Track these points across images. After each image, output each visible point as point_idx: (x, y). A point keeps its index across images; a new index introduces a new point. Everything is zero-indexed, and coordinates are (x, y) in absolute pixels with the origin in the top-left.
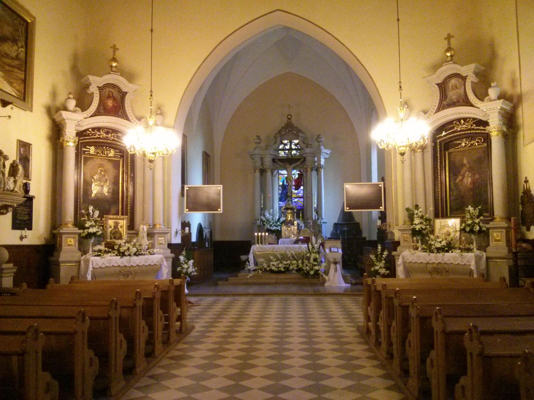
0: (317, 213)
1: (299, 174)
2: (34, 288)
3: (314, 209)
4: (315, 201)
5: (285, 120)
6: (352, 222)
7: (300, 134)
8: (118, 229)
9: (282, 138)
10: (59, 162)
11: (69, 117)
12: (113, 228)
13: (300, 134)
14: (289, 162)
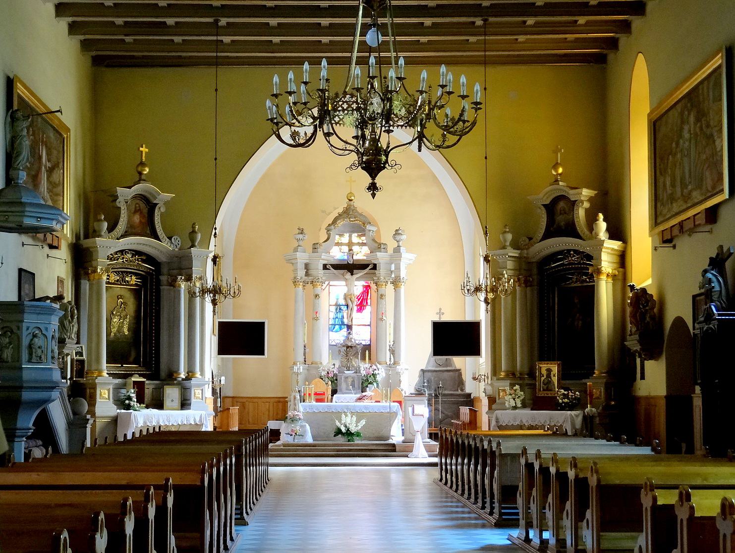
0: (393, 352)
3: (388, 348)
4: (390, 330)
6: (449, 368)
7: (368, 227)
8: (551, 378)
10: (497, 340)
11: (628, 344)
12: (545, 377)
13: (368, 227)
14: (350, 267)
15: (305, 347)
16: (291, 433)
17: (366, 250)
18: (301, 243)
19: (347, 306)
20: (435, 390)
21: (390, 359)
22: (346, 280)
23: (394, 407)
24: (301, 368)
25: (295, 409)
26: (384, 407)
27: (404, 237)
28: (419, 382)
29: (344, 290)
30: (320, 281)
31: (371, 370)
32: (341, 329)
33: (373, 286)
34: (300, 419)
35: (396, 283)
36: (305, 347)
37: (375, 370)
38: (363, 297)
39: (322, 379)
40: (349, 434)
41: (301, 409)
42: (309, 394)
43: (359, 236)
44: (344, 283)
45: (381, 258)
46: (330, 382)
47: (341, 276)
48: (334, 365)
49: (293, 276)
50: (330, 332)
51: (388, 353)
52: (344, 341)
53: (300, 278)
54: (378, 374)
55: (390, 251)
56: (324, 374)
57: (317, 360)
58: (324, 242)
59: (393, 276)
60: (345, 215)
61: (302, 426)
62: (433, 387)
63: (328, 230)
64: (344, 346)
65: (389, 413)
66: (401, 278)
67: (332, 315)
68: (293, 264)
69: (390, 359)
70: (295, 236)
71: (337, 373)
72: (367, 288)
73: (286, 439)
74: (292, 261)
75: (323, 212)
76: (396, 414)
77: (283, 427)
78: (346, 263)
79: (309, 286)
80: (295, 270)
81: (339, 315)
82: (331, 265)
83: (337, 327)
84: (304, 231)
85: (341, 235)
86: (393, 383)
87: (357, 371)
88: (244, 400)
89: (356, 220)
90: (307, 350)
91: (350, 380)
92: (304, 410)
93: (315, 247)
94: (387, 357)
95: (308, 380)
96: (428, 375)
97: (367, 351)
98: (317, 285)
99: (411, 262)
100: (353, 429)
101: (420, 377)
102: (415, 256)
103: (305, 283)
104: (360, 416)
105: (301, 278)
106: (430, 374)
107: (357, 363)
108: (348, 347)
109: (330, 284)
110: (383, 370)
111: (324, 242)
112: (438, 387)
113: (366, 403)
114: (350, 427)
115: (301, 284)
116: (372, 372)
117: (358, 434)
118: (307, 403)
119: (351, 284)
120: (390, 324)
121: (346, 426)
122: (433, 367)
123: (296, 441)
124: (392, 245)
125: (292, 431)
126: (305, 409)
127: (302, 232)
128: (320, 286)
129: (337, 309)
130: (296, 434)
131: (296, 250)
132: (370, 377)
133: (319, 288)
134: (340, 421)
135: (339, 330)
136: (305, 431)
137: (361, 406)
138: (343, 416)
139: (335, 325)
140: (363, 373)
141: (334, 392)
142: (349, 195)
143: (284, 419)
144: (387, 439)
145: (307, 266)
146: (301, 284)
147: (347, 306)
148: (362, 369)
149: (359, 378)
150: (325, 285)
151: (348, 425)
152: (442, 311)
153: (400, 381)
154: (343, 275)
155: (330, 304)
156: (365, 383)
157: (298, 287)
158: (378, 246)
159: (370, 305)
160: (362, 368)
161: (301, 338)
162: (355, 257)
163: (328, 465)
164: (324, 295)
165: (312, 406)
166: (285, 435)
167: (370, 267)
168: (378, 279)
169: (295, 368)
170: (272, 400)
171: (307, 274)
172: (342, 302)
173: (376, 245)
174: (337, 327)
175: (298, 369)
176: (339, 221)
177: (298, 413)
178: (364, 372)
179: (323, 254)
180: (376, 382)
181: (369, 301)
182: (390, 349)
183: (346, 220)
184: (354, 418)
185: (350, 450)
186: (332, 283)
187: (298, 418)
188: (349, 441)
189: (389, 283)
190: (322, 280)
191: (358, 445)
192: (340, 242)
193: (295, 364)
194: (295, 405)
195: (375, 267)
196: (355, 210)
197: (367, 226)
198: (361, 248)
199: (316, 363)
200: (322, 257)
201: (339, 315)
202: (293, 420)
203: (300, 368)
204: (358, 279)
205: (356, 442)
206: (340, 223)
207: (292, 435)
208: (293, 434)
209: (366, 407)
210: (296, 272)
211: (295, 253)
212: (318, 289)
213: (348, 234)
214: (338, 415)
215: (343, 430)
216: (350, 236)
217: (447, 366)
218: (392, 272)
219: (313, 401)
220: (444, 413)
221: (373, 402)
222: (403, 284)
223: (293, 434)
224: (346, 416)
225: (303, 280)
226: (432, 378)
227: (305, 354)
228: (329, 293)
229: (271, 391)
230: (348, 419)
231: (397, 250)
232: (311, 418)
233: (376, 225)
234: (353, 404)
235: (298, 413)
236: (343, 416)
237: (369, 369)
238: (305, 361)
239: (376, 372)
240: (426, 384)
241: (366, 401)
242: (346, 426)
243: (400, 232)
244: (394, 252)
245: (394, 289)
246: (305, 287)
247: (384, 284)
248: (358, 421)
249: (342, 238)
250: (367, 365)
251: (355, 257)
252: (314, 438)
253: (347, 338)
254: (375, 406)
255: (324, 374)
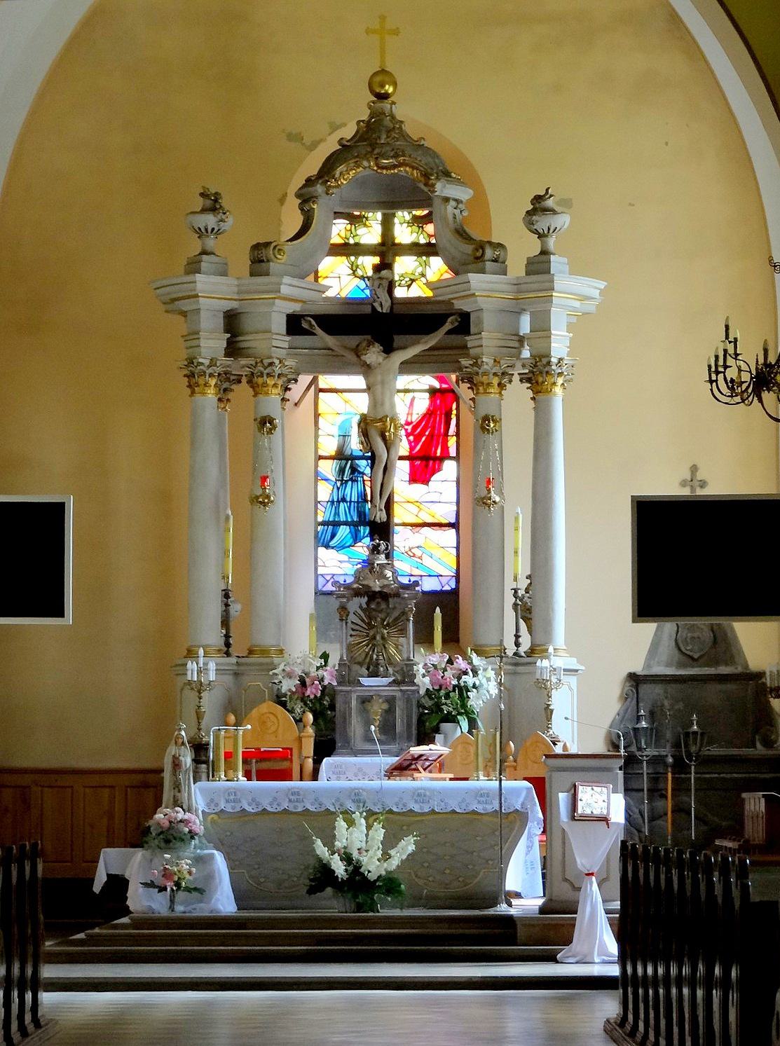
0: (525, 612)
1: (433, 392)
2: (394, 77)
3: (509, 600)
4: (518, 540)
5: (359, 109)
6: (724, 670)
7: (442, 188)
9: (331, 701)
13: (442, 188)
14: (374, 328)
15: (227, 596)
16: (160, 881)
17: (437, 268)
18: (211, 243)
19: (373, 459)
20: (677, 745)
21: (517, 637)
22: (366, 370)
23: (516, 791)
24: (212, 666)
25: (176, 803)
26: (481, 794)
27: (562, 221)
28: (622, 716)
29: (361, 403)
30: (277, 370)
31: (449, 674)
32: (356, 539)
33: (464, 391)
34: (192, 835)
35: (538, 375)
36: (227, 596)
37: (465, 673)
38: (433, 428)
39: (283, 704)
40: (358, 885)
41: (199, 802)
42: (228, 755)
43: (419, 222)
44: (358, 381)
45: (484, 289)
46: (310, 717)
47: (351, 357)
48: (325, 656)
49: (184, 354)
50: (322, 550)
51: (510, 615)
52: (358, 576)
53: (207, 362)
54: (474, 686)
55: (516, 268)
56: (288, 685)
57: (266, 639)
58: (291, 240)
59: (526, 353)
60: (363, 148)
61: (199, 860)
62: (669, 735)
63: (306, 199)
64: (357, 593)
65: (498, 813)
66: (554, 360)
67: (325, 492)
68: (184, 314)
69: (517, 637)
70: (191, 217)
71: (335, 683)
72: (442, 399)
73: (146, 903)
74: (179, 305)
75: (295, 137)
76: (518, 819)
77: (133, 865)
78: (368, 310)
79: (243, 389)
80: (193, 335)
81: (352, 492)
82: (315, 317)
83: (343, 531)
84: (224, 202)
85: (355, 220)
86: (524, 714)
87: (406, 676)
88: (26, 780)
89: (401, 165)
90: (235, 609)
91: (378, 708)
92: (208, 805)
93: (260, 257)
94: (509, 630)
95: (235, 708)
96: (651, 692)
97: (438, 610)
98: (265, 385)
99: (590, 306)
100: (373, 867)
101: (625, 698)
102: (602, 285)
103: (227, 381)
104: (397, 823)
105: (213, 362)
106: (658, 690)
107: (404, 649)
108: (372, 596)
109: (322, 385)
110: (491, 674)
111: (291, 240)
112: (687, 735)
113: (423, 780)
114: (364, 860)
115: (213, 382)
116: (455, 682)
117: (389, 884)
118: (221, 784)
119: (383, 383)
120: (517, 519)
121: (347, 858)
122: (668, 665)
123: (179, 908)
124: (520, 247)
125: (167, 874)
126: (210, 802)
127: (213, 204)
128: (275, 391)
129: (341, 471)
130: (178, 884)
131: (193, 267)
132: (447, 696)
133: (275, 394)
134: (329, 841)
135: (350, 542)
136: (210, 877)
137: (404, 791)
138: (341, 824)
139: (336, 524)
140: (424, 682)
141: (324, 748)
142: (378, 79)
143: (137, 837)
144: (494, 902)
145: (232, 322)
146: (213, 382)
147: (373, 459)
148: (420, 669)
149: (408, 701)
150: (297, 390)
151: (355, 855)
152: (699, 476)
153: (548, 712)
154: (357, 352)
155: (321, 453)
156: (432, 716)
157: (204, 394)
158: (473, 252)
159: (457, 458)
160: (421, 666)
161: (212, 569)
162: (400, 293)
163: (339, 983)
164: (294, 422)
165: (235, 792)
166: (141, 889)
167: (448, 326)
168: (475, 364)
169: (192, 666)
170: (126, 780)
171: (233, 350)
172: (355, 445)
173: (469, 249)
174: (343, 531)
175: (199, 672)
176: (342, 168)
177: (187, 816)
178: (427, 680)
179: (287, 280)
180: (469, 714)
181: (452, 442)
182: (515, 605)
183: (365, 163)
184: (379, 833)
185: (273, 940)
186: (325, 381)
187: (187, 830)
188: (359, 908)
189: (516, 378)
190: (285, 370)
191: (390, 922)
192: (352, 241)
193: (191, 654)
194: (177, 786)
195: (464, 324)
196: (396, 128)
197: (438, 186)
198: (426, 264)
199: (265, 652)
200: (285, 290)
201: (352, 492)
202: (172, 838)
203: (207, 668)
204: (408, 367)
205: (384, 912)
206: (347, 175)
207: (165, 889)
208: (170, 885)
209: (419, 795)
210: (194, 343)
211: (189, 278)
212: (271, 403)
213: (379, 215)
214: (323, 822)
215: (339, 868)
216: (387, 224)
217: (716, 663)
218: (521, 340)
219: (240, 774)
220: (705, 823)
221: (446, 780)
222: (560, 381)
223: (170, 885)
224: (351, 823)
225: (219, 370)
226: (666, 703)
227: (225, 622)
228: (317, 416)
229: (104, 746)
230: (355, 835)
231: (539, 265)
232: (236, 833)
233: (470, 179)
234: (376, 784)
235: (187, 816)
236: (341, 824)
237: (445, 670)
238: (228, 645)
239: (469, 680)
240: (644, 724)
241: (424, 774)
242: (347, 858)
243: (550, 203)
244: (528, 273)
245: (533, 399)
246: (230, 396)
247: (495, 381)
248: (390, 842)
249: (361, 231)
250: (437, 657)
251: (400, 293)
252: (241, 898)
253: (369, 564)
254: (452, 789)
255: (288, 685)
